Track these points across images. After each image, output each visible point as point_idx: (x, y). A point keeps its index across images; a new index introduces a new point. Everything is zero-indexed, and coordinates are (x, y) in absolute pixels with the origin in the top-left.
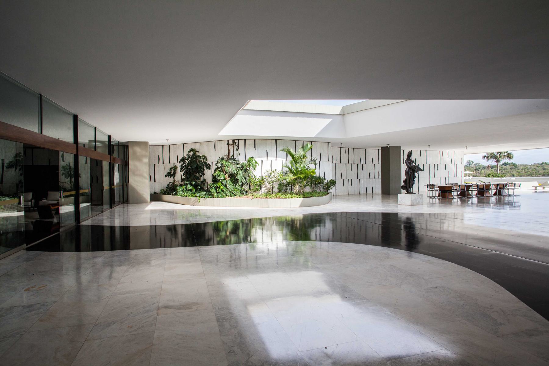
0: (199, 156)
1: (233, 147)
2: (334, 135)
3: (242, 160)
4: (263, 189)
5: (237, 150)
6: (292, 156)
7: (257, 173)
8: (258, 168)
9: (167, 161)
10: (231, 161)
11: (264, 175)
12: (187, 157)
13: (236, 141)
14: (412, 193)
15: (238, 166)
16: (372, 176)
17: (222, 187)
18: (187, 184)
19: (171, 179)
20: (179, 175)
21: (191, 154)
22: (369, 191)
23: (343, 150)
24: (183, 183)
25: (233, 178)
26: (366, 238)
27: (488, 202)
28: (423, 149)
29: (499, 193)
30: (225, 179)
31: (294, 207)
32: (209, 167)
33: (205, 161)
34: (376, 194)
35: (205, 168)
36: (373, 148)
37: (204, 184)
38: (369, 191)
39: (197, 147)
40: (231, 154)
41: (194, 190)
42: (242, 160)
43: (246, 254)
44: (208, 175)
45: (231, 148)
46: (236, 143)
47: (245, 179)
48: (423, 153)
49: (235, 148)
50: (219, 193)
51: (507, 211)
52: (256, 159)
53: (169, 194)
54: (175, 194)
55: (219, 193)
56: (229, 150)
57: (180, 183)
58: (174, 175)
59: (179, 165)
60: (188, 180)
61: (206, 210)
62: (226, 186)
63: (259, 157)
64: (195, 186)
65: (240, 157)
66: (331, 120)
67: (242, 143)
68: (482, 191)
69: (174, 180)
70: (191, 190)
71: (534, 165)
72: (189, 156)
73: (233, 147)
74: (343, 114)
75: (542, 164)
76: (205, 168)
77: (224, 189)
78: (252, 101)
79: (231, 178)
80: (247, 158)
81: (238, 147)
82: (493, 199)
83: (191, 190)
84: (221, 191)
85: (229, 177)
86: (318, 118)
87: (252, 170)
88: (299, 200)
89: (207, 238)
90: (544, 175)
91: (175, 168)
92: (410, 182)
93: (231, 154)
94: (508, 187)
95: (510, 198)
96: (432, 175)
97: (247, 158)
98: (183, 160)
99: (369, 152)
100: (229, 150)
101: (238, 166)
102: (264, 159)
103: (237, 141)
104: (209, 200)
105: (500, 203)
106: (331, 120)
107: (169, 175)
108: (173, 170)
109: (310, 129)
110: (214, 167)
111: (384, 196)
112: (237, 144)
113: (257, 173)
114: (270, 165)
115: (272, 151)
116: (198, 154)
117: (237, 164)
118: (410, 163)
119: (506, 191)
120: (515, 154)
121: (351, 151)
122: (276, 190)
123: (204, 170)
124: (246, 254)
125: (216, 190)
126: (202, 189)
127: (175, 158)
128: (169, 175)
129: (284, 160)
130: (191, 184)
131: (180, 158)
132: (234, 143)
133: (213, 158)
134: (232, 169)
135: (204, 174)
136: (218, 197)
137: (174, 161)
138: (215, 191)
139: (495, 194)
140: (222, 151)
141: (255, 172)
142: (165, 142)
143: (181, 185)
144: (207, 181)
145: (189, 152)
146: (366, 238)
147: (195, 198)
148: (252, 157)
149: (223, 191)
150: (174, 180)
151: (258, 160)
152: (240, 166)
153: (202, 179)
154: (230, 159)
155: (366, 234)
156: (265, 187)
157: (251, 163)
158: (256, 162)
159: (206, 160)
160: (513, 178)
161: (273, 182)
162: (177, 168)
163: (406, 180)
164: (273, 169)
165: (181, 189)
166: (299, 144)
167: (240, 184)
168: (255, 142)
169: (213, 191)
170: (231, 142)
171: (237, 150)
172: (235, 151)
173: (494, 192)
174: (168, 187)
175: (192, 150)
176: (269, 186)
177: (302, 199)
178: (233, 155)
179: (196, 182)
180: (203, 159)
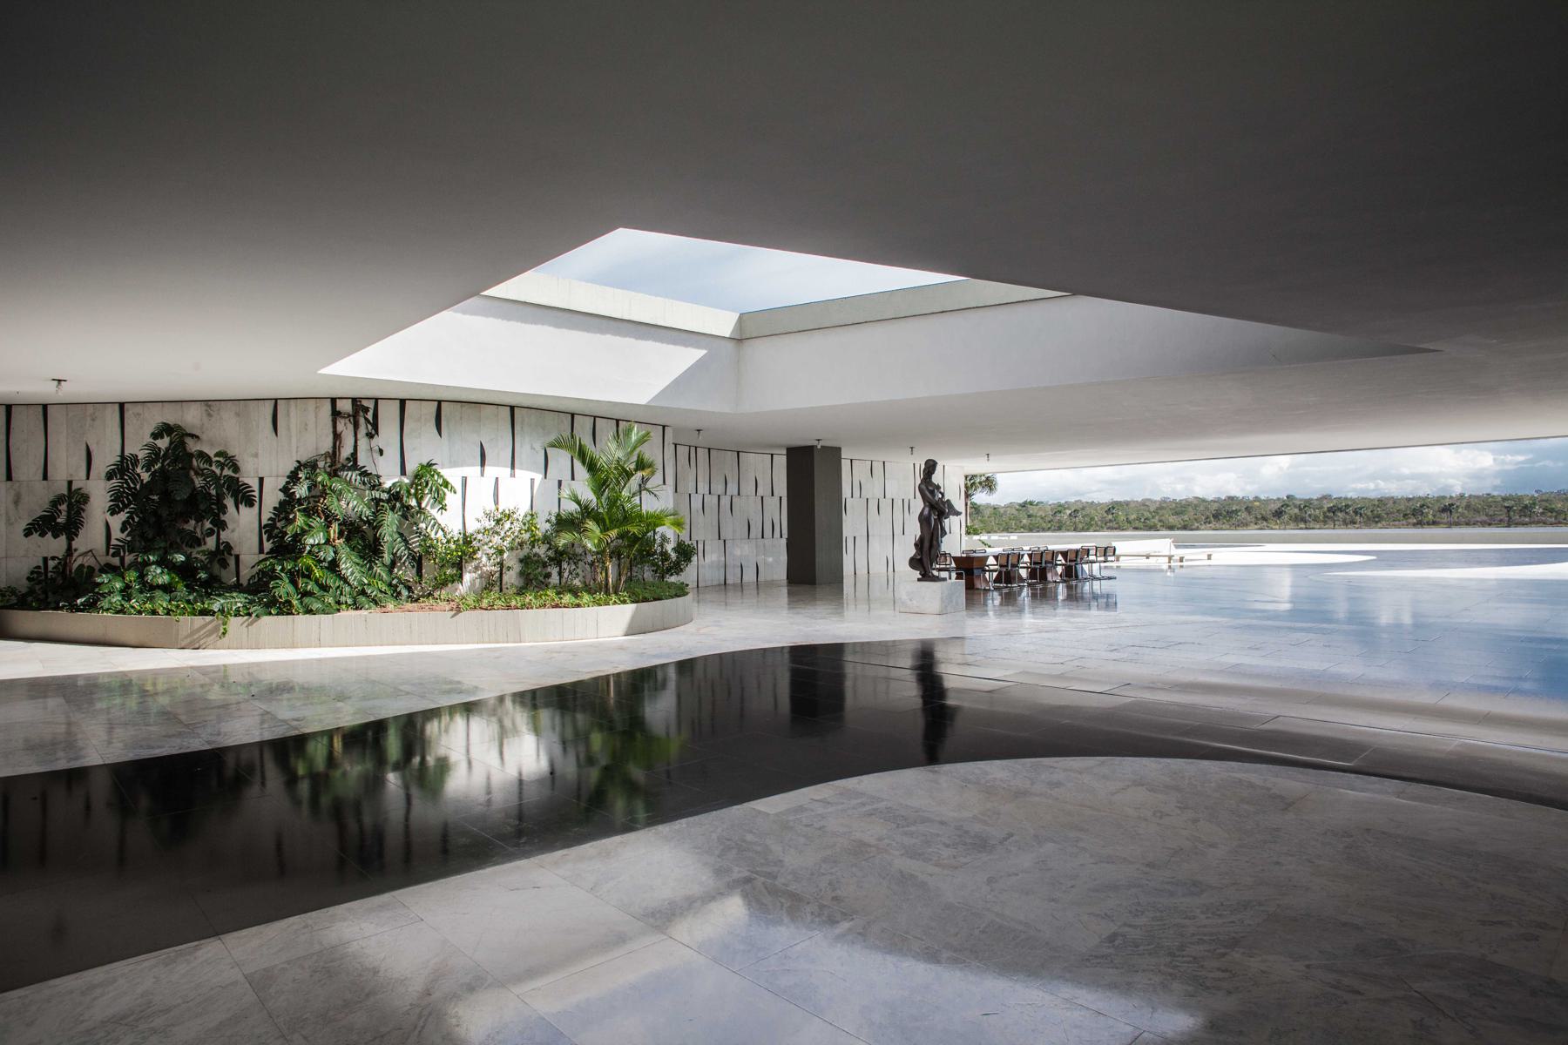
0: (202, 455)
1: (356, 426)
2: (712, 406)
3: (390, 478)
4: (467, 577)
5: (370, 436)
6: (592, 467)
7: (449, 520)
8: (452, 500)
9: (27, 469)
10: (353, 476)
11: (470, 530)
12: (141, 455)
13: (365, 403)
14: (936, 579)
15: (376, 494)
16: (756, 531)
17: (317, 573)
18: (147, 564)
19: (55, 546)
20: (102, 524)
21: (163, 443)
22: (750, 576)
23: (682, 451)
24: (116, 561)
25: (364, 539)
26: (742, 716)
27: (1056, 598)
28: (879, 457)
29: (1070, 573)
30: (328, 542)
31: (596, 636)
32: (245, 497)
33: (227, 472)
34: (771, 584)
35: (229, 502)
36: (765, 447)
37: (224, 564)
38: (750, 576)
39: (191, 418)
40: (346, 451)
41: (180, 586)
42: (390, 478)
43: (407, 818)
44: (243, 528)
45: (345, 428)
46: (366, 410)
47: (406, 541)
48: (878, 467)
49: (362, 431)
50: (306, 594)
51: (1093, 617)
52: (443, 472)
53: (44, 605)
54: (91, 606)
55: (306, 594)
56: (337, 436)
57: (103, 560)
58: (72, 527)
59: (100, 494)
60: (147, 551)
61: (258, 664)
62: (333, 566)
63: (454, 464)
64: (186, 572)
65: (380, 460)
66: (703, 352)
67: (388, 415)
68: (1040, 570)
69: (70, 551)
70: (167, 589)
71: (1011, 505)
72: (155, 454)
73: (356, 426)
74: (740, 338)
75: (1024, 505)
76: (229, 502)
77: (331, 581)
78: (621, 231)
79: (348, 540)
80: (412, 467)
81: (375, 426)
82: (1062, 590)
83: (167, 589)
84: (316, 590)
85: (341, 534)
86: (662, 341)
87: (434, 512)
88: (620, 614)
89: (229, 771)
90: (1031, 530)
91: (76, 501)
92: (931, 546)
93: (346, 451)
94: (1092, 558)
95: (1096, 584)
96: (898, 530)
97: (412, 467)
98: (123, 467)
99: (749, 459)
100: (337, 436)
101: (376, 494)
102: (472, 471)
103: (370, 405)
104: (270, 623)
105: (1074, 597)
106: (703, 352)
107: (42, 525)
108: (64, 507)
109: (635, 378)
110: (272, 498)
111: (795, 588)
112: (370, 416)
113: (449, 520)
114: (492, 496)
115: (499, 449)
116: (193, 446)
117: (373, 487)
118: (932, 492)
119: (1086, 567)
120: (1001, 479)
121: (702, 453)
122: (511, 577)
123: (223, 509)
124: (407, 818)
125: (294, 583)
126: (213, 586)
127: (88, 466)
128: (42, 525)
129: (539, 477)
130: (163, 562)
131: (107, 457)
132: (360, 412)
133: (267, 464)
134: (351, 504)
135: (222, 525)
136: (309, 611)
137: (67, 466)
138: (291, 588)
139: (998, 580)
140: (311, 438)
141: (442, 519)
142: (41, 390)
143: (108, 568)
144: (236, 551)
145: (155, 436)
146: (742, 716)
147: (199, 621)
148: (430, 465)
149: (325, 588)
150: (70, 551)
151: (452, 475)
152: (385, 496)
153: (211, 543)
154: (344, 468)
155: (742, 709)
156: (476, 568)
157: (425, 479)
158: (446, 484)
159: (236, 469)
160: (1014, 537)
161: (501, 552)
162: (85, 499)
163: (922, 539)
164: (505, 505)
165: (118, 585)
166: (606, 430)
167: (387, 558)
168: (443, 410)
169: (284, 589)
170: (345, 406)
171: (370, 436)
172: (363, 442)
173: (1059, 570)
174: (36, 575)
175: (165, 430)
176: (489, 566)
177: (630, 608)
178: (354, 455)
179: (188, 557)
180: (222, 466)
